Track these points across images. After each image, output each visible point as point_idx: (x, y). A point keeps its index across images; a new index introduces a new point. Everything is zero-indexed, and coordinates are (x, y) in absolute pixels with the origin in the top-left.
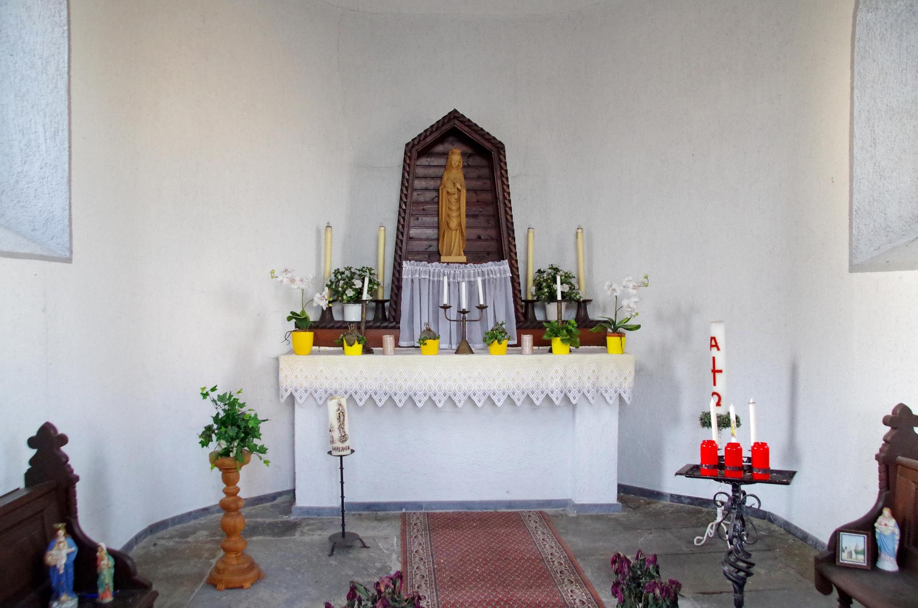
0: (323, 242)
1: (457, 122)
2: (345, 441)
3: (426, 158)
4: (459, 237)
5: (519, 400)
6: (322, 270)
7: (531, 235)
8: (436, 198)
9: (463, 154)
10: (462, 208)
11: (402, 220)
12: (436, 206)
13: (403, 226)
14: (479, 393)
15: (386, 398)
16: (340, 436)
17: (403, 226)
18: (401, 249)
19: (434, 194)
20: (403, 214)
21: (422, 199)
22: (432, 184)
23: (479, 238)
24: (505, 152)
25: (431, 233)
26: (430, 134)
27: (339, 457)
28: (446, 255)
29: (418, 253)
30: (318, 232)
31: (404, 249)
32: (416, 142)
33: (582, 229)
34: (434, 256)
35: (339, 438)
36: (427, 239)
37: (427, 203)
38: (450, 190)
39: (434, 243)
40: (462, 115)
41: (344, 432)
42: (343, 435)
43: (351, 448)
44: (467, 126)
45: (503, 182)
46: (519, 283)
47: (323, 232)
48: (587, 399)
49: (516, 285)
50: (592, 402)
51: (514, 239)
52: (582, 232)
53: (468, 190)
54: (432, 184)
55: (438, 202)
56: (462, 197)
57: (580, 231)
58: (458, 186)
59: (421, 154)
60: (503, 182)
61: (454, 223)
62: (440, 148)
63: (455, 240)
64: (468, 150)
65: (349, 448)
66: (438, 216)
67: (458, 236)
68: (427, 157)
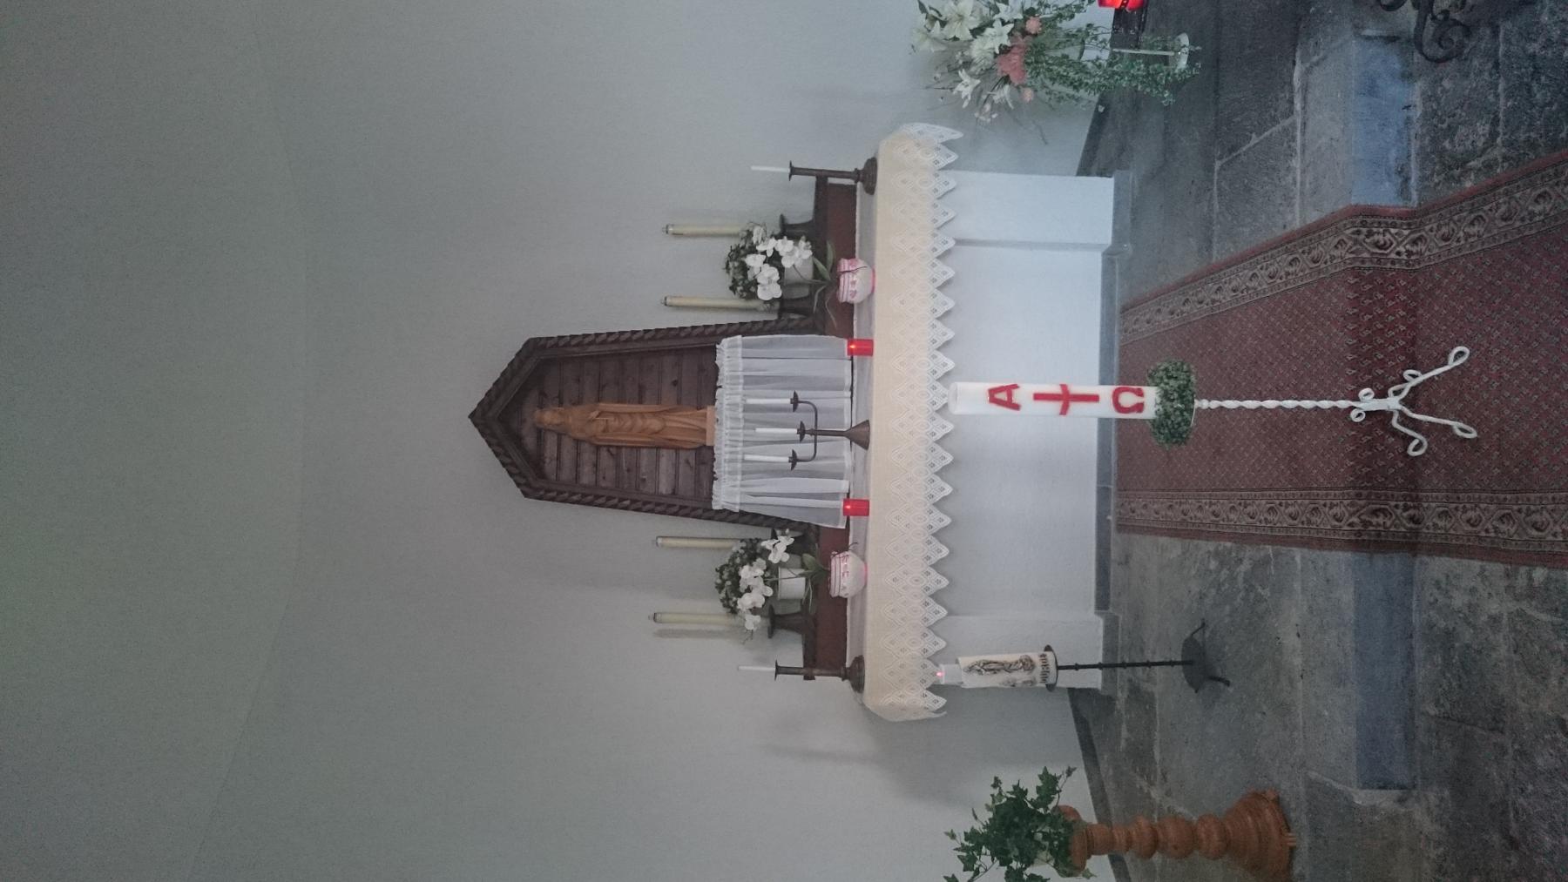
0: (677, 627)
1: (490, 414)
2: (1031, 661)
3: (546, 465)
4: (680, 416)
5: (945, 273)
6: (721, 628)
7: (676, 302)
8: (611, 449)
9: (541, 406)
10: (629, 410)
11: (648, 507)
12: (624, 450)
13: (658, 504)
14: (932, 365)
15: (939, 449)
16: (1022, 670)
17: (658, 504)
18: (694, 509)
19: (604, 453)
20: (639, 505)
21: (611, 474)
22: (588, 456)
23: (675, 383)
24: (541, 338)
25: (666, 459)
26: (509, 457)
27: (1060, 671)
28: (705, 438)
29: (698, 482)
30: (662, 634)
31: (695, 504)
32: (523, 481)
33: (667, 227)
34: (704, 457)
35: (1027, 672)
36: (676, 467)
37: (618, 466)
38: (602, 428)
39: (682, 453)
40: (479, 404)
41: (1017, 662)
42: (1021, 665)
43: (1042, 652)
44: (497, 397)
45: (590, 343)
46: (754, 323)
47: (661, 627)
48: (946, 223)
49: (756, 327)
50: (951, 215)
51: (682, 329)
52: (673, 225)
53: (599, 400)
54: (588, 456)
55: (618, 447)
56: (612, 409)
57: (671, 229)
58: (594, 414)
59: (542, 475)
60: (590, 343)
61: (654, 424)
62: (530, 441)
63: (680, 422)
64: (534, 396)
65: (1044, 656)
66: (640, 447)
67: (676, 418)
68: (544, 463)
